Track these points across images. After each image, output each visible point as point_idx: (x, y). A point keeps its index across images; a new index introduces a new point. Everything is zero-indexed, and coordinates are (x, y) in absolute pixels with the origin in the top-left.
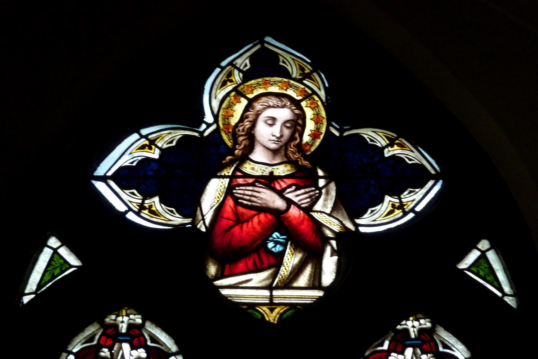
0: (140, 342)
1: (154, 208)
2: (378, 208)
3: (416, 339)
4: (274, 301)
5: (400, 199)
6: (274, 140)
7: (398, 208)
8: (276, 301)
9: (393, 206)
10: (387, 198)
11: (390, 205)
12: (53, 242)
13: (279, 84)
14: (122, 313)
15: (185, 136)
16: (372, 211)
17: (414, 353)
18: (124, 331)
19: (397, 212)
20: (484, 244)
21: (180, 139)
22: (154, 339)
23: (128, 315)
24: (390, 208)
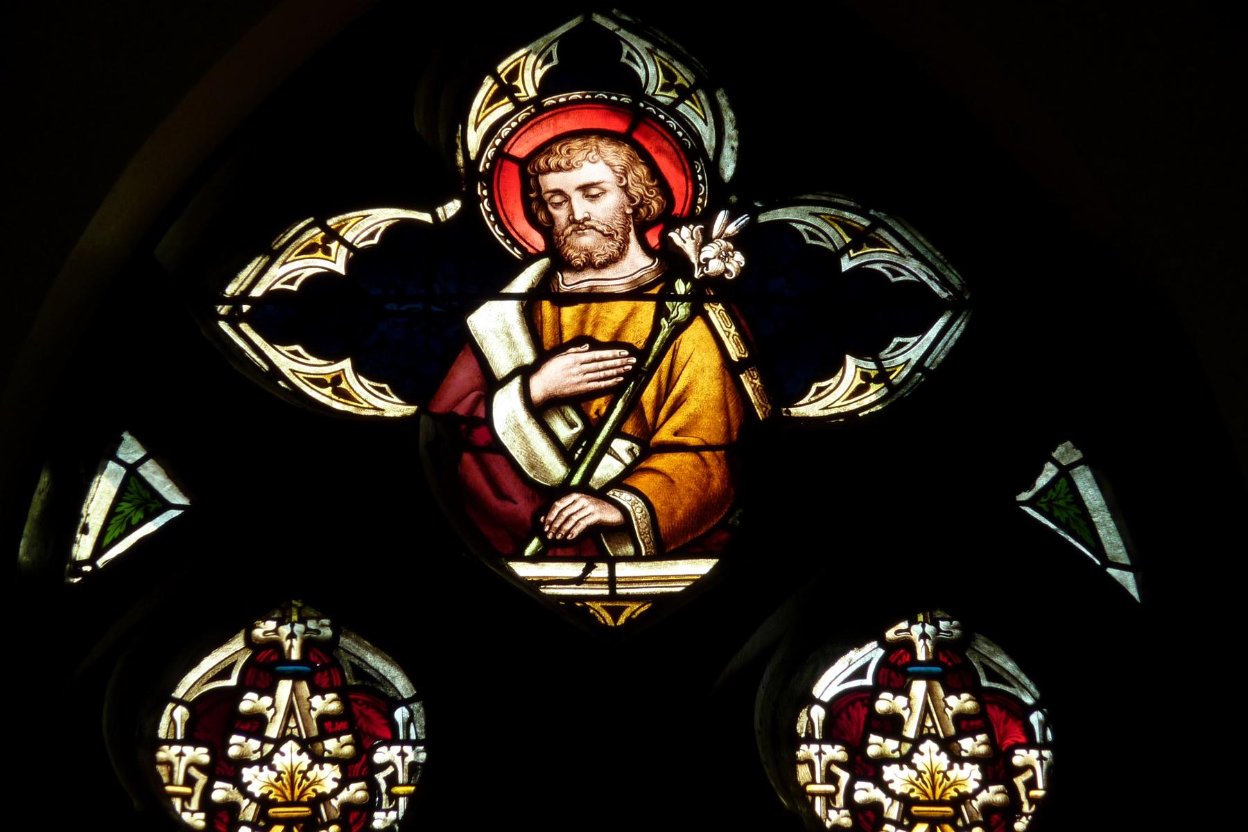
0: (331, 682)
1: (343, 385)
2: (833, 381)
3: (927, 663)
4: (618, 591)
5: (878, 362)
6: (601, 232)
7: (877, 380)
8: (621, 591)
9: (865, 376)
10: (850, 361)
11: (858, 375)
12: (131, 450)
13: (542, 216)
14: (290, 617)
15: (404, 222)
16: (820, 390)
17: (930, 690)
18: (295, 655)
19: (874, 387)
20: (1065, 452)
21: (388, 229)
22: (361, 671)
23: (302, 620)
24: (859, 381)
